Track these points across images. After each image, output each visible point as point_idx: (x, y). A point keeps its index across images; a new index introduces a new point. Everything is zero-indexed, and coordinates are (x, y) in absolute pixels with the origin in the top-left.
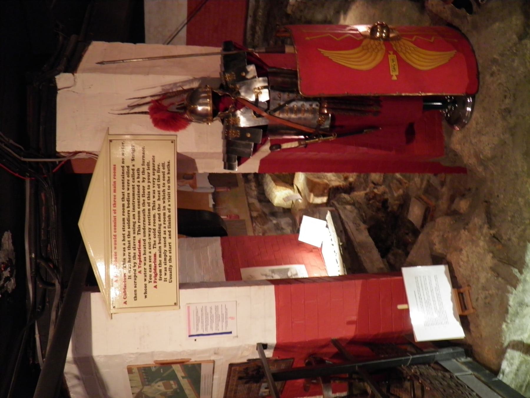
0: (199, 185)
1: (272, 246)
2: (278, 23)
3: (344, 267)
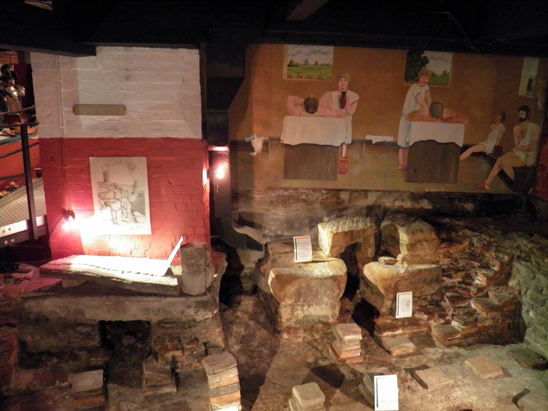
0: (415, 125)
1: (185, 203)
3: (97, 275)
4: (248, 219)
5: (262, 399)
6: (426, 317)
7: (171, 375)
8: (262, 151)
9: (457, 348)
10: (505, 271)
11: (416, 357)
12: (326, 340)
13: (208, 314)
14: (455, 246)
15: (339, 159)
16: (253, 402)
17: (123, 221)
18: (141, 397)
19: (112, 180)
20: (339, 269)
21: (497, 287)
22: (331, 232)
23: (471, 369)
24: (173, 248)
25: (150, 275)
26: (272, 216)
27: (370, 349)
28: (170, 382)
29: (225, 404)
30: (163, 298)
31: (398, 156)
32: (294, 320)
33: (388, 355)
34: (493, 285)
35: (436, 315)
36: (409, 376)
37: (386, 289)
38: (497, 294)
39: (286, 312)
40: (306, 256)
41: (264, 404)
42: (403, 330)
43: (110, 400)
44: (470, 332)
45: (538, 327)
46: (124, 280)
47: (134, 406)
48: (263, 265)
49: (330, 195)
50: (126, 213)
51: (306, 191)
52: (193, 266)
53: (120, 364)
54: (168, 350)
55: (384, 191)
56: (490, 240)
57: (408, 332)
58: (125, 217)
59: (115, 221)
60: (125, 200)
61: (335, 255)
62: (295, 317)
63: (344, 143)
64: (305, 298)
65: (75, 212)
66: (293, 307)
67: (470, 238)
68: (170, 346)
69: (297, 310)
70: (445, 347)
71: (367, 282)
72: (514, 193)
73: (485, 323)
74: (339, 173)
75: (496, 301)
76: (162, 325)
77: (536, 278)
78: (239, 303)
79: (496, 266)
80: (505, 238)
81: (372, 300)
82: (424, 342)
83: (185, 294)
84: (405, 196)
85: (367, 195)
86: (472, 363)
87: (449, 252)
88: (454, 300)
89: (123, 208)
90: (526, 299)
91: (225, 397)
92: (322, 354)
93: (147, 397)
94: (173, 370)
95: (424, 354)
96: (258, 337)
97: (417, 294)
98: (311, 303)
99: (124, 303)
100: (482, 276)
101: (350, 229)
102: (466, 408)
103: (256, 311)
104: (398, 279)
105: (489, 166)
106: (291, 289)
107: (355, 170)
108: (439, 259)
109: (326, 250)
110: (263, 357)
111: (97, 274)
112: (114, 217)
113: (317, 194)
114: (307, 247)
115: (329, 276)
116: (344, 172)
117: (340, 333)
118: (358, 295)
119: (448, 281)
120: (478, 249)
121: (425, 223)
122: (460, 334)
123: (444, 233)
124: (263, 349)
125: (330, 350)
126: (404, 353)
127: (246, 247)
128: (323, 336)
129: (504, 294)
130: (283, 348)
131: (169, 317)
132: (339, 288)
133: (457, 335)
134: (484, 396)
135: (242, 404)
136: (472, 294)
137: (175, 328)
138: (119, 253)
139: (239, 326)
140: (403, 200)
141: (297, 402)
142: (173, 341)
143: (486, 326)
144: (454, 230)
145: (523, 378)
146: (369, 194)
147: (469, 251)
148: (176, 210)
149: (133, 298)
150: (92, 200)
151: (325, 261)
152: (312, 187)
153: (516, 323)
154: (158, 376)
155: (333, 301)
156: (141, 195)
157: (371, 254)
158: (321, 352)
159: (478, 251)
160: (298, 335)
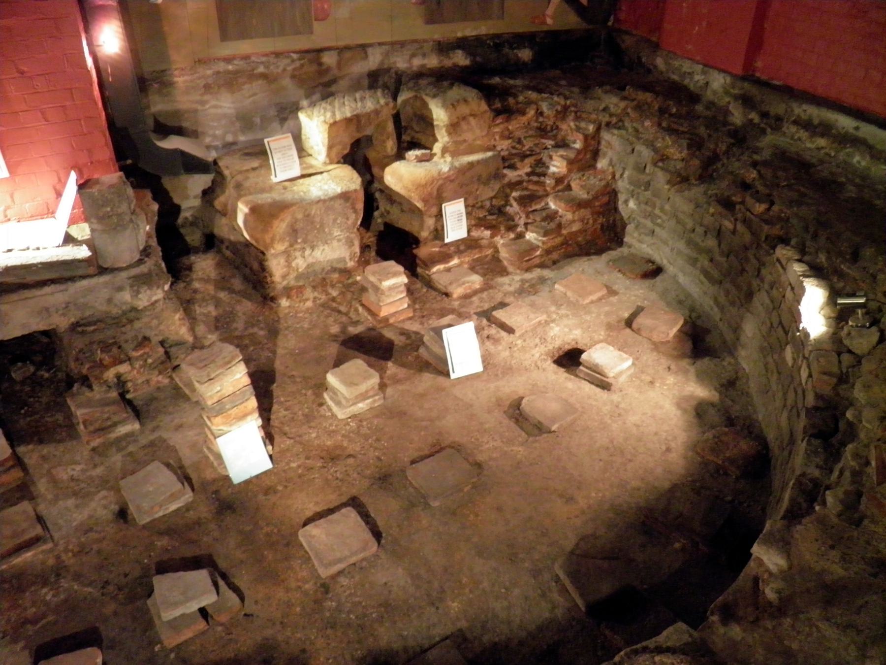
2: (776, 208)
4: (171, 123)
5: (282, 403)
6: (488, 233)
9: (539, 270)
10: (591, 148)
11: (486, 293)
12: (349, 296)
13: (156, 294)
14: (516, 119)
20: (349, 181)
21: (582, 173)
22: (325, 122)
23: (565, 294)
24: (59, 194)
25: (34, 250)
26: (212, 111)
27: (417, 295)
28: (125, 415)
29: (235, 423)
30: (70, 283)
32: (293, 276)
33: (446, 299)
34: (575, 171)
35: (502, 228)
36: (485, 322)
37: (425, 201)
38: (584, 183)
39: (279, 264)
40: (291, 169)
41: (286, 409)
42: (459, 258)
43: (31, 471)
44: (553, 244)
45: (642, 220)
48: (218, 196)
49: (306, 60)
51: (264, 59)
52: (109, 217)
53: (23, 411)
55: (392, 44)
56: (566, 104)
57: (467, 259)
61: (336, 160)
62: (293, 270)
64: (304, 236)
66: (287, 254)
67: (536, 104)
68: (107, 359)
69: (296, 258)
70: (523, 272)
71: (391, 196)
72: (591, 27)
73: (571, 228)
74: (316, 20)
75: (583, 194)
76: (80, 329)
77: (635, 151)
78: (190, 268)
79: (578, 141)
80: (586, 98)
81: (404, 222)
82: (492, 271)
83: (106, 269)
84: (427, 47)
85: (366, 53)
86: (565, 286)
87: (508, 130)
88: (524, 201)
90: (622, 185)
91: (234, 412)
92: (349, 318)
93: (94, 450)
94: (122, 395)
95: (496, 288)
96: (240, 314)
97: (471, 202)
98: (315, 243)
100: (560, 159)
101: (355, 113)
104: (441, 182)
106: (281, 226)
110: (260, 343)
113: (283, 63)
115: (336, 194)
116: (323, 17)
117: (372, 279)
118: (378, 219)
119: (511, 175)
120: (549, 120)
121: (469, 89)
123: (497, 101)
124: (255, 330)
125: (360, 309)
126: (469, 291)
127: (182, 171)
128: (344, 290)
129: (592, 182)
130: (286, 322)
131: (87, 313)
132: (355, 211)
134: (589, 327)
136: (548, 189)
137: (104, 329)
139: (204, 304)
140: (424, 55)
141: (339, 394)
142: (110, 351)
145: (632, 293)
146: (370, 51)
149: (14, 297)
151: (321, 173)
152: (271, 49)
154: (102, 412)
157: (392, 149)
158: (346, 314)
160: (304, 298)
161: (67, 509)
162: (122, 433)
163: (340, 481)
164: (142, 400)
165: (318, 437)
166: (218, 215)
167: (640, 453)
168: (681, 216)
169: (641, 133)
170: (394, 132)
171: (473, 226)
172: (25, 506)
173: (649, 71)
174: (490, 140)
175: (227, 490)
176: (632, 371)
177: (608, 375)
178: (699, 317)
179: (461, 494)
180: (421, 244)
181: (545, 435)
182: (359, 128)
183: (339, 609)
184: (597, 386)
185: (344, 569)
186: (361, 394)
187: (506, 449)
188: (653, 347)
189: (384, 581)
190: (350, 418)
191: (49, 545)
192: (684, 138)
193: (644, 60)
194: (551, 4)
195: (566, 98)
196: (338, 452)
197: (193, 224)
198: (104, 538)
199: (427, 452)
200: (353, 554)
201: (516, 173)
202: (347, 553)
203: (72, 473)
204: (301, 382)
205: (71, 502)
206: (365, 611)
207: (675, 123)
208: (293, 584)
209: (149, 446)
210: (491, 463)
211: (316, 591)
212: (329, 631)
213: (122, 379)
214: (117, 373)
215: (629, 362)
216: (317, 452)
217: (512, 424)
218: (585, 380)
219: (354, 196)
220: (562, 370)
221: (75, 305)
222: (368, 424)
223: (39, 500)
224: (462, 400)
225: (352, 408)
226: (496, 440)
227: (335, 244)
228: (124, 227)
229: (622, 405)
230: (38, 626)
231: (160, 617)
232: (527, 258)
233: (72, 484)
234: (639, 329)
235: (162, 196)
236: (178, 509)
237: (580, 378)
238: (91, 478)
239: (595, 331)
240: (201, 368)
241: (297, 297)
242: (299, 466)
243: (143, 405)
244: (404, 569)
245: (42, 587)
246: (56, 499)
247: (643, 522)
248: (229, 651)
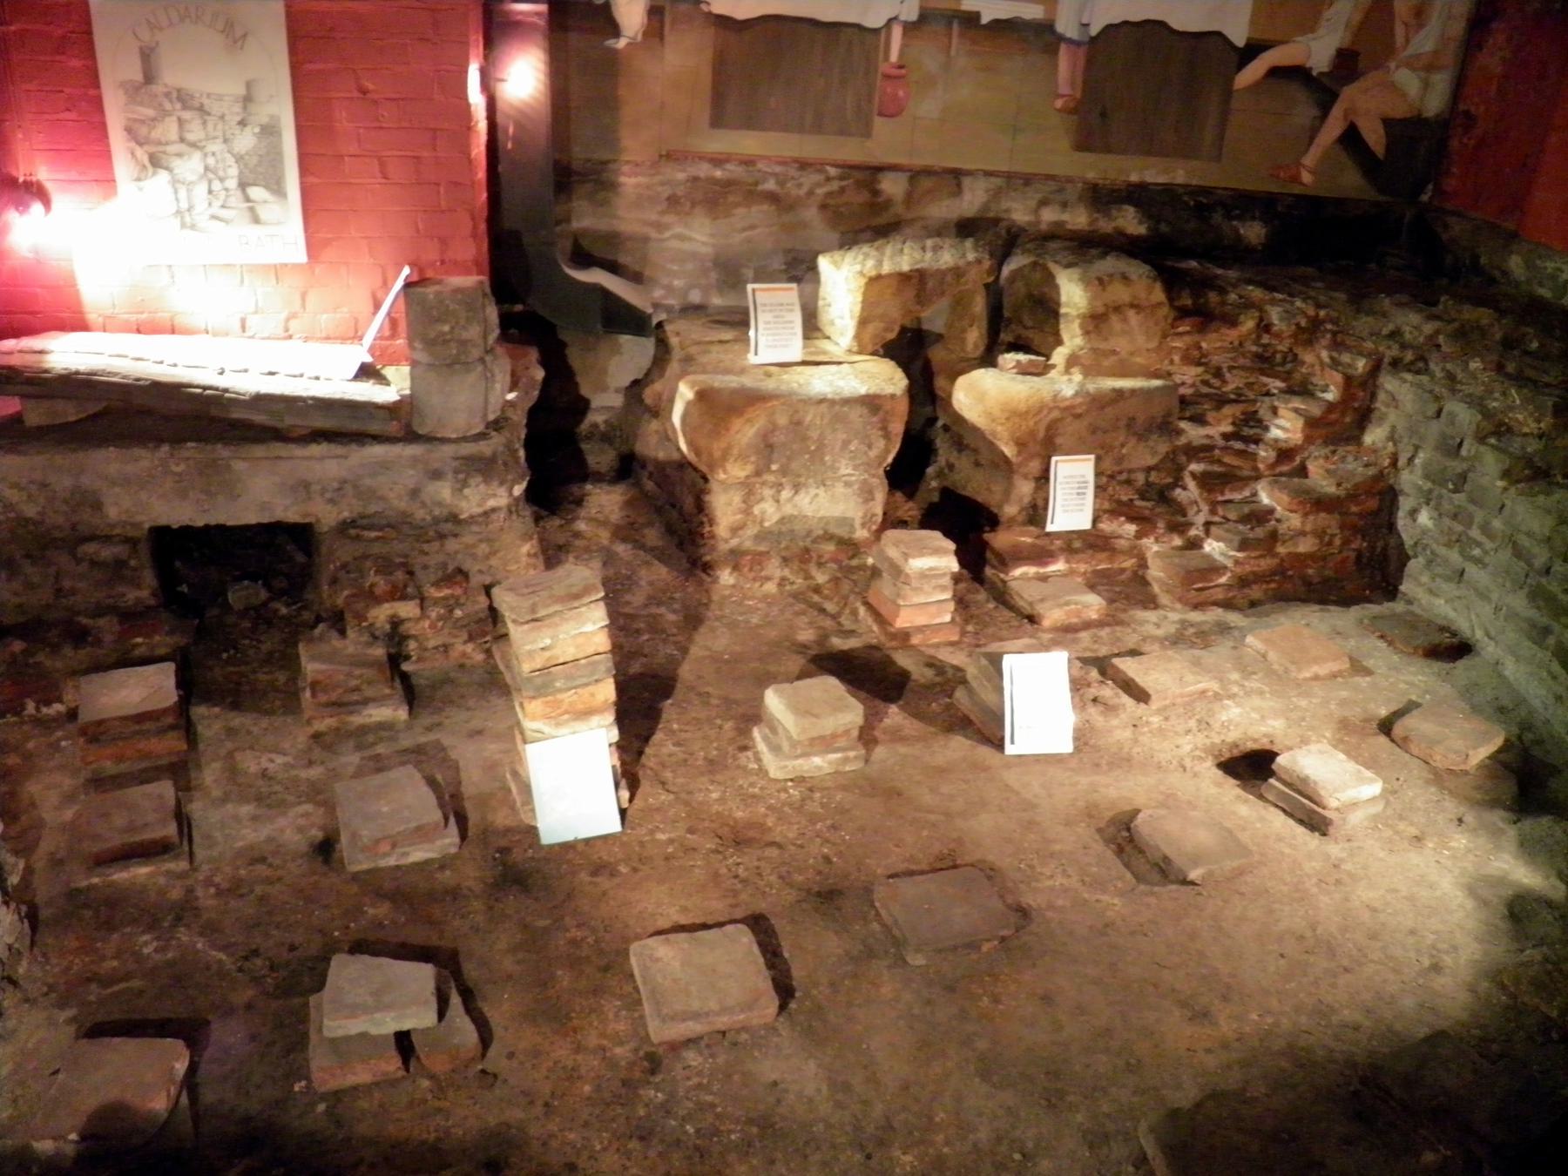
1: (414, 157)
3: (138, 380)
4: (598, 251)
5: (673, 732)
6: (1131, 528)
7: (388, 673)
8: (645, 34)
9: (1220, 610)
10: (1356, 405)
11: (1107, 630)
13: (495, 495)
14: (1216, 331)
15: (880, 70)
16: (647, 739)
17: (214, 217)
18: (301, 738)
19: (172, 76)
21: (1332, 448)
22: (861, 273)
23: (1264, 656)
24: (377, 306)
26: (675, 244)
27: (974, 610)
28: (387, 691)
29: (567, 721)
30: (354, 447)
31: (1056, 66)
32: (751, 531)
33: (1028, 626)
34: (1320, 441)
35: (1161, 525)
36: (1094, 674)
37: (1021, 444)
38: (1333, 467)
41: (677, 744)
42: (1068, 561)
43: (201, 746)
44: (1255, 569)
45: (1442, 551)
46: (226, 390)
47: (280, 760)
50: (224, 192)
51: (778, 169)
52: (445, 342)
53: (225, 656)
54: (376, 599)
55: (1009, 176)
56: (1317, 315)
57: (1082, 568)
58: (220, 203)
59: (188, 219)
60: (216, 147)
61: (870, 348)
62: (754, 522)
63: (895, 18)
64: (784, 460)
65: (50, 186)
67: (1261, 310)
69: (762, 499)
72: (1382, 198)
73: (1296, 545)
74: (881, 114)
76: (353, 532)
78: (579, 502)
79: (1332, 387)
80: (1358, 311)
81: (976, 485)
82: (1127, 598)
84: (1072, 193)
85: (959, 185)
86: (1266, 641)
87: (1200, 348)
89: (211, 176)
90: (1409, 480)
91: (567, 697)
92: (839, 624)
93: (316, 736)
96: (643, 583)
98: (802, 480)
99: (229, 467)
100: (1293, 415)
101: (918, 266)
102: (1256, 746)
103: (631, 520)
104: (1056, 414)
105: (1315, 112)
106: (745, 432)
107: (927, 107)
108: (1170, 368)
109: (842, 334)
110: (663, 631)
111: (138, 375)
112: (184, 205)
113: (810, 179)
114: (789, 317)
116: (892, 111)
118: (932, 482)
119: (1193, 433)
122: (1229, 574)
124: (662, 610)
125: (862, 611)
126: (1075, 620)
128: (839, 575)
129: (1350, 467)
132: (887, 436)
133: (1221, 575)
134: (1303, 719)
135: (621, 720)
136: (1261, 466)
138: (203, 327)
139: (586, 556)
140: (1064, 205)
141: (780, 730)
142: (391, 573)
143: (1301, 554)
144: (1213, 287)
146: (967, 182)
147: (1254, 348)
148: (384, 181)
149: (259, 451)
150: (108, 145)
151: (840, 363)
152: (796, 155)
153: (1379, 550)
154: (349, 675)
155: (866, 476)
156: (270, 131)
157: (976, 346)
158: (834, 617)
159: (1280, 348)
160: (763, 574)
161: (236, 818)
162: (373, 719)
163: (741, 881)
164: (427, 679)
165: (722, 800)
166: (646, 416)
167: (1372, 961)
168: (1524, 541)
169: (1461, 383)
170: (985, 314)
171: (1105, 511)
172: (165, 789)
173: (1492, 281)
174: (1162, 361)
175: (526, 851)
176: (1379, 807)
177: (1325, 802)
178: (1540, 742)
179: (974, 956)
180: (1000, 528)
181: (1174, 887)
182: (922, 298)
183: (666, 1109)
184: (1301, 822)
185: (701, 1038)
186: (822, 738)
187: (1086, 896)
188: (1432, 777)
189: (774, 1076)
190: (791, 780)
191: (183, 865)
192: (1550, 395)
193: (1483, 260)
194: (1314, 145)
195: (1319, 306)
196: (751, 834)
197: (606, 438)
198: (280, 879)
199: (924, 867)
200: (724, 1010)
201: (1203, 431)
202: (713, 1005)
203: (265, 763)
204: (718, 706)
205: (246, 810)
206: (717, 1123)
207: (1534, 368)
208: (593, 1040)
209: (413, 752)
210: (1049, 914)
211: (631, 1065)
212: (634, 1145)
213: (403, 629)
214: (393, 616)
215: (1374, 788)
216: (713, 825)
217: (1109, 854)
218: (1277, 806)
219: (888, 407)
220: (1232, 781)
221: (355, 487)
222: (823, 797)
223: (197, 794)
224: (1018, 793)
225: (800, 761)
226: (1069, 876)
227: (840, 489)
228: (467, 366)
229: (1348, 866)
230: (109, 991)
231: (320, 1030)
232: (1200, 585)
233: (260, 782)
234: (1406, 739)
235: (560, 375)
236: (427, 862)
237: (1267, 801)
238: (296, 781)
239: (1312, 728)
240: (523, 595)
241: (751, 570)
242: (671, 841)
243: (427, 686)
244: (819, 1066)
245: (143, 932)
246: (225, 799)
247: (1355, 1093)
248: (428, 1126)
